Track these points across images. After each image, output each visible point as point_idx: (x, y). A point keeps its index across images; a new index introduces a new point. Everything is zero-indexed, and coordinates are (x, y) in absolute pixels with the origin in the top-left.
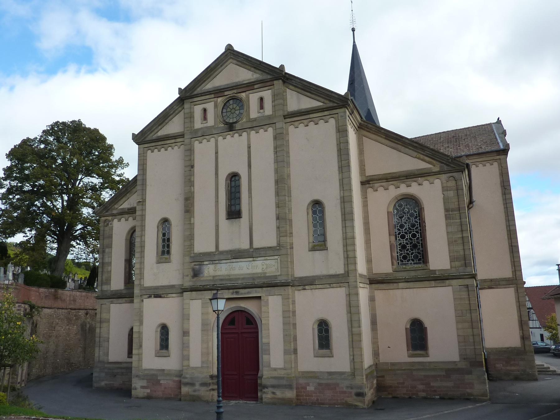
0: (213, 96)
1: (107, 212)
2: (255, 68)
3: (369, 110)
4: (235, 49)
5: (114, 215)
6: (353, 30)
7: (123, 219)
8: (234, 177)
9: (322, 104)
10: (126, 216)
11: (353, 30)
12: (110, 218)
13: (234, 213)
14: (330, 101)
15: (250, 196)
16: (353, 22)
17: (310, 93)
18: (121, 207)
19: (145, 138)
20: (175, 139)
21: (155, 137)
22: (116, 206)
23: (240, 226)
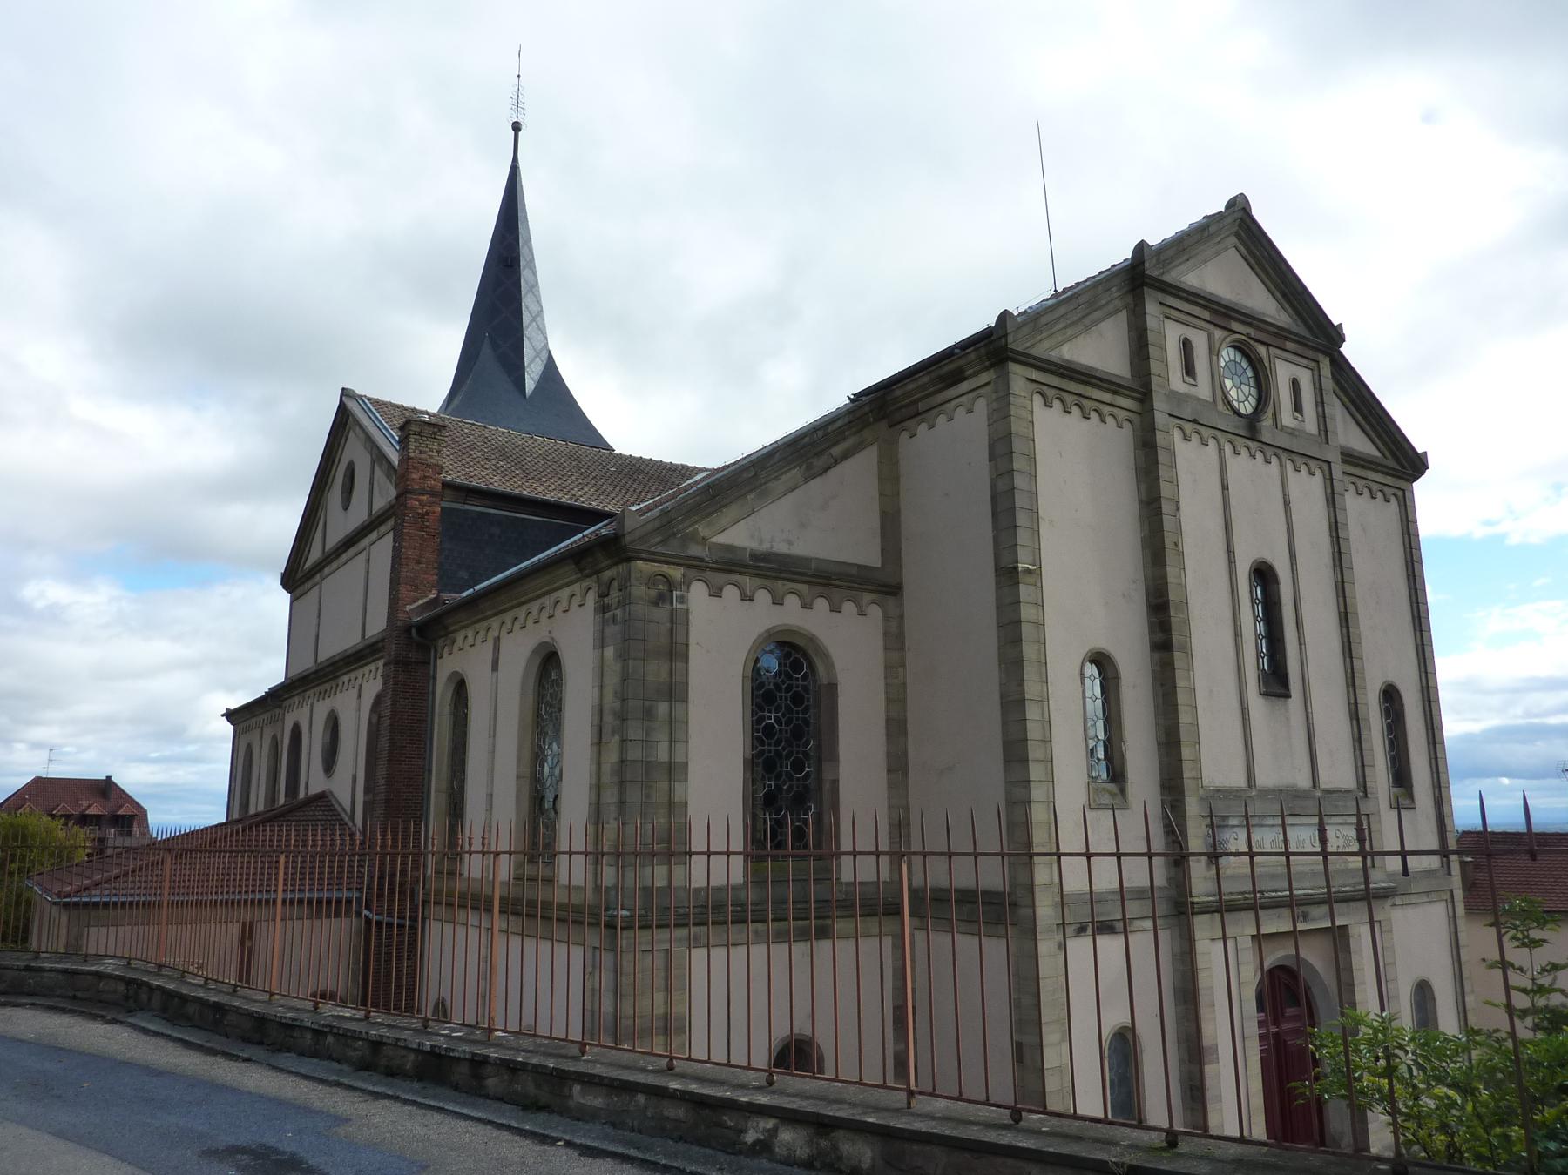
0: (1206, 315)
1: (664, 542)
2: (1284, 295)
3: (550, 357)
4: (1256, 213)
5: (698, 566)
6: (516, 127)
7: (731, 592)
8: (1263, 575)
9: (1377, 454)
10: (747, 581)
11: (516, 127)
12: (676, 573)
13: (1276, 681)
14: (1394, 455)
15: (1301, 642)
16: (518, 106)
17: (1365, 417)
18: (721, 539)
19: (1032, 346)
20: (1115, 393)
21: (1054, 355)
22: (702, 530)
23: (1288, 719)
